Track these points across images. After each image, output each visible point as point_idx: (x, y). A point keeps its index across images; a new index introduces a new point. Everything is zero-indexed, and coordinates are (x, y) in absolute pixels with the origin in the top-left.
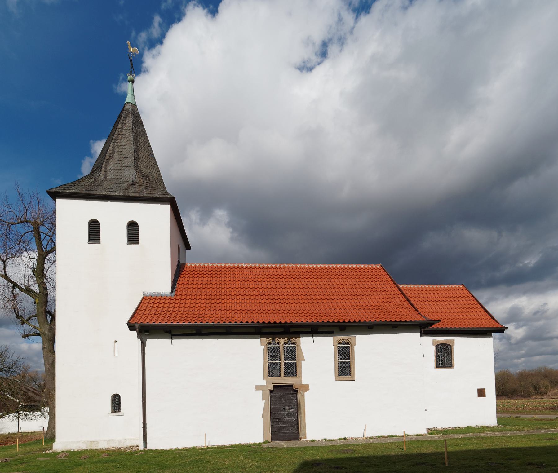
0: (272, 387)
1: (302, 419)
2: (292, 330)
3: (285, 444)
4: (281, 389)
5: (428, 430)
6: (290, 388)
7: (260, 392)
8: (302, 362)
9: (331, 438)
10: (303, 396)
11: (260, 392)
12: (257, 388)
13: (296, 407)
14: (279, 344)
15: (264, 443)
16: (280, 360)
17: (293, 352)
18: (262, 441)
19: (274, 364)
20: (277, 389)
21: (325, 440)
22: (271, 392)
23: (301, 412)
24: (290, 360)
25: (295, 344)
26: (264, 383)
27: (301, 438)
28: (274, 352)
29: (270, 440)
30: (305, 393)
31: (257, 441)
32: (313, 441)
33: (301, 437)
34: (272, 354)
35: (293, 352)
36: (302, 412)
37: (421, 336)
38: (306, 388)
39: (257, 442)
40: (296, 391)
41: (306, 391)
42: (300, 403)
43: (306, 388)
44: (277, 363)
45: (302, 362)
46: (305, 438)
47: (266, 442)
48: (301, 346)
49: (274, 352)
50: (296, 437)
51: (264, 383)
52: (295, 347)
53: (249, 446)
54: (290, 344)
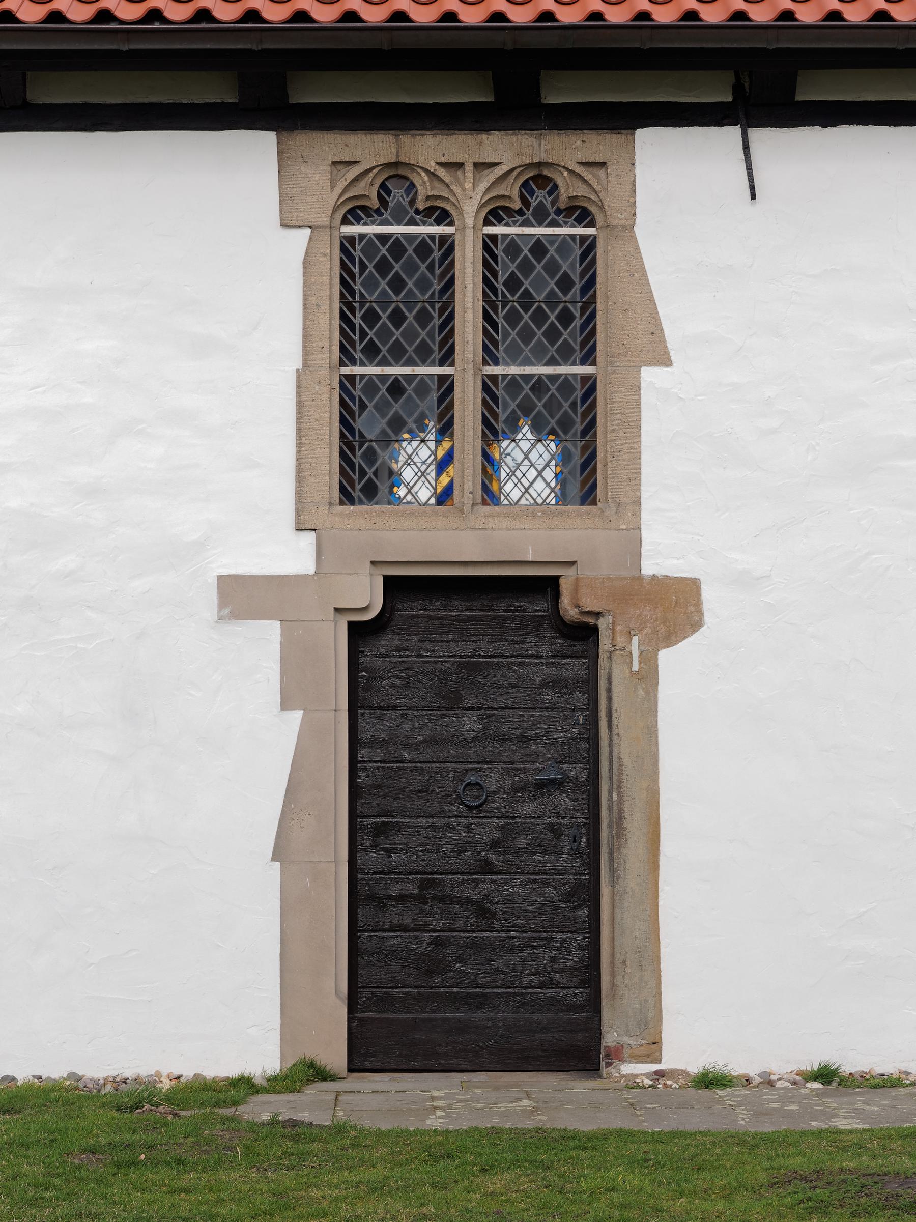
0: (369, 597)
1: (632, 879)
2: (558, 92)
3: (443, 1102)
4: (458, 608)
5: (274, 858)
6: (534, 607)
7: (267, 636)
8: (650, 376)
9: (887, 1066)
10: (648, 677)
11: (267, 636)
12: (241, 597)
13: (578, 772)
14: (444, 217)
15: (279, 1084)
16: (447, 358)
17: (565, 283)
18: (263, 1058)
19: (396, 387)
20: (412, 609)
21: (826, 1075)
22: (360, 633)
23: (619, 821)
24: (539, 356)
25: (584, 216)
26: (296, 556)
27: (616, 1054)
28: (397, 284)
29: (334, 1053)
30: (666, 657)
31: (222, 1066)
32: (710, 1081)
33: (609, 1039)
34: (379, 307)
35: (565, 283)
36: (634, 825)
37: (665, 360)
38: (676, 608)
39: (210, 1072)
40: (583, 634)
41: (672, 637)
42: (620, 744)
43: (676, 608)
44: (422, 385)
45: (650, 376)
46: (652, 1049)
47: (306, 1073)
48: (639, 231)
49: (397, 284)
50: (579, 1050)
51: (296, 556)
52: (589, 247)
53: (134, 1101)
54: (541, 217)
